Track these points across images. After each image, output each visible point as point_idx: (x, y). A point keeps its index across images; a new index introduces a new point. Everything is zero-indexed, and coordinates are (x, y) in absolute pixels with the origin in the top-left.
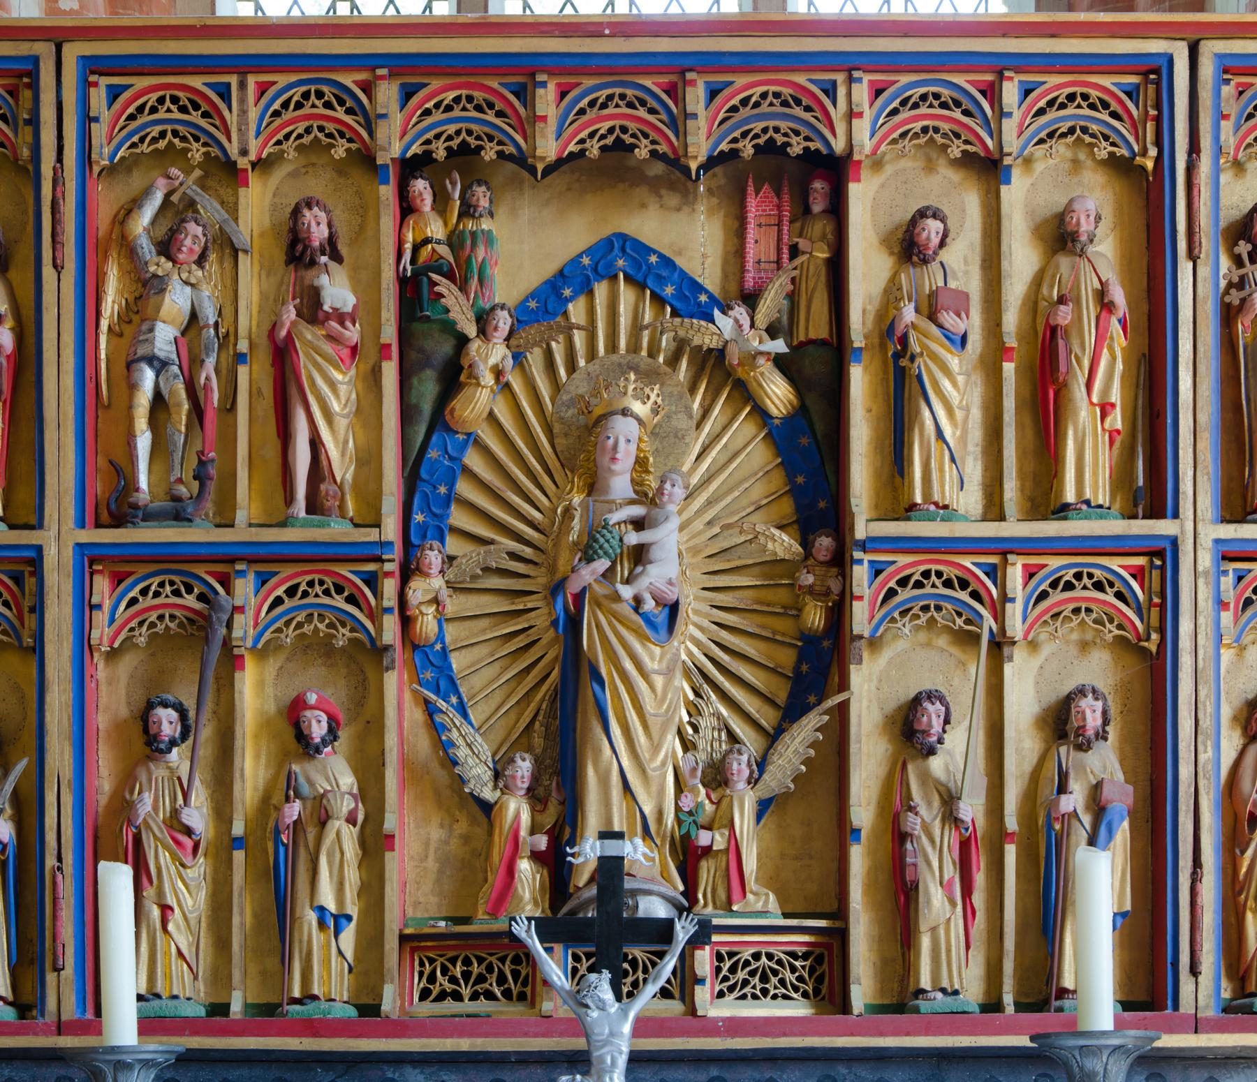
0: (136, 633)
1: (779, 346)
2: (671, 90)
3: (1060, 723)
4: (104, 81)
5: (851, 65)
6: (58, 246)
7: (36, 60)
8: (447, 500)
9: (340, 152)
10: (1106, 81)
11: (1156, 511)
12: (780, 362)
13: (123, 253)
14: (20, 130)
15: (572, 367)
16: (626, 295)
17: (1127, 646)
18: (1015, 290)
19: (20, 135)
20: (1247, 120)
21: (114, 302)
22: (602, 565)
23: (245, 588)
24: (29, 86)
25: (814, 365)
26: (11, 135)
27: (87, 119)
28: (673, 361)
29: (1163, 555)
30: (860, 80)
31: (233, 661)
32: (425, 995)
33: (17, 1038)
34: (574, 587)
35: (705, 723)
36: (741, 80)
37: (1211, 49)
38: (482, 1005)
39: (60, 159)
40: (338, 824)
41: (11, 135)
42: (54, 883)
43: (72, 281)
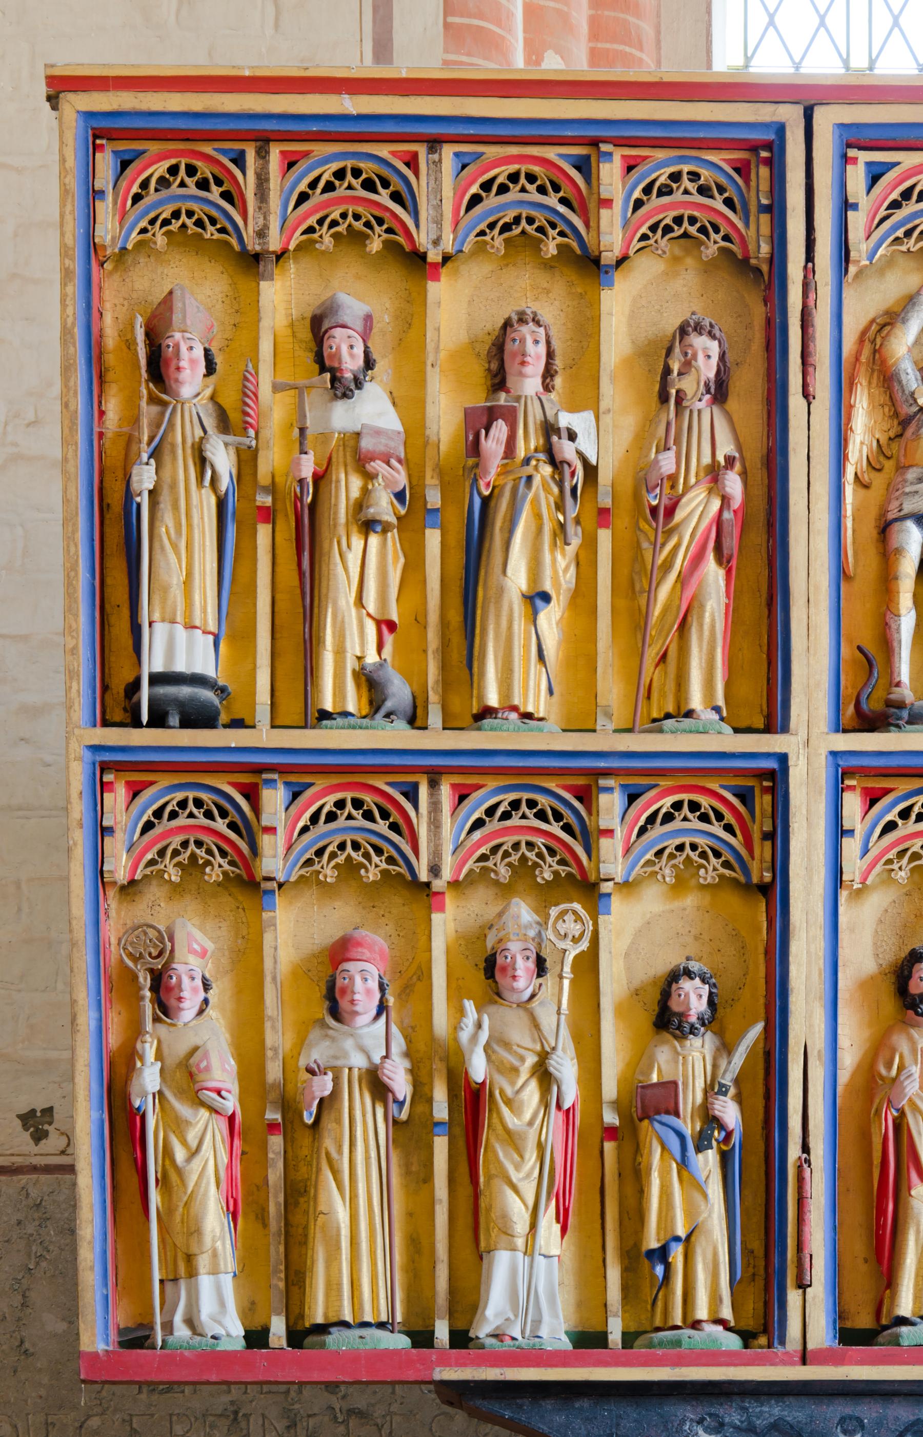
0: (895, 866)
2: (583, 166)
4: (864, 157)
6: (811, 369)
7: (781, 129)
9: (551, 248)
13: (875, 381)
14: (752, 219)
19: (753, 226)
20: (469, 208)
21: (862, 443)
24: (768, 162)
26: (740, 225)
27: (846, 206)
30: (855, 160)
33: (881, 1368)
39: (810, 256)
41: (740, 225)
42: (800, 1180)
43: (827, 414)
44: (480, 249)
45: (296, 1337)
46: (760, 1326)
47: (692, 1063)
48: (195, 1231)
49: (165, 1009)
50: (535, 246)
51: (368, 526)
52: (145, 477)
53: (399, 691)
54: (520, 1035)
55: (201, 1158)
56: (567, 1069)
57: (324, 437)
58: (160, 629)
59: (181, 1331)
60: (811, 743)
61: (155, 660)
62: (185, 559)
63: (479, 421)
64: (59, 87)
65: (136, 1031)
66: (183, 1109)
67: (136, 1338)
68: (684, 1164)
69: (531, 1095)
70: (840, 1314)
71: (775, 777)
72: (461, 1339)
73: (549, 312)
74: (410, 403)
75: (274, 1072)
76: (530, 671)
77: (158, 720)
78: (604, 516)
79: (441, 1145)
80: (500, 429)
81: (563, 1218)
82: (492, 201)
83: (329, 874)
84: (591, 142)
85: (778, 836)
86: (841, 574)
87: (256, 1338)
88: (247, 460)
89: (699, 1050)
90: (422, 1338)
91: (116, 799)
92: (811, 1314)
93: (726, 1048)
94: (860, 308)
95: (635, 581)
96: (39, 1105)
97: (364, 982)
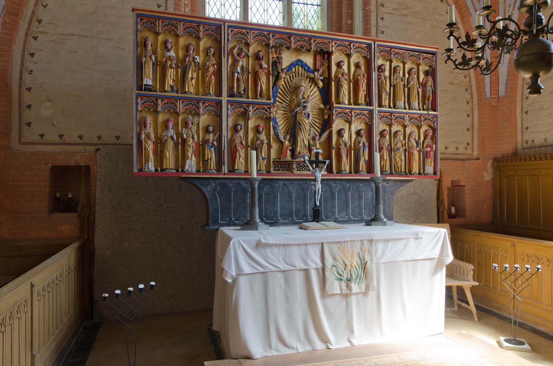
1: (322, 78)
2: (198, 26)
3: (358, 133)
5: (159, 18)
8: (276, 96)
10: (363, 45)
11: (370, 105)
12: (322, 80)
15: (293, 78)
16: (300, 68)
17: (366, 124)
18: (352, 73)
22: (300, 108)
23: (251, 108)
25: (326, 81)
27: (228, 35)
28: (307, 78)
29: (371, 112)
31: (249, 119)
32: (274, 170)
34: (296, 111)
35: (311, 131)
36: (318, 40)
37: (377, 43)
38: (283, 172)
40: (265, 144)
44: (185, 35)
45: (162, 170)
46: (219, 170)
47: (211, 137)
48: (149, 156)
49: (145, 127)
50: (192, 35)
51: (172, 68)
52: (144, 59)
53: (175, 88)
54: (190, 133)
55: (150, 147)
56: (196, 137)
57: (166, 56)
58: (145, 79)
59: (147, 169)
60: (225, 98)
61: (145, 83)
62: (149, 70)
63: (185, 56)
64: (133, 10)
65: (141, 130)
66: (148, 141)
67: (140, 170)
68: (210, 149)
69: (191, 140)
70: (228, 168)
71: (221, 102)
72: (182, 171)
73: (193, 43)
74: (177, 53)
75: (159, 136)
76: (191, 87)
77: (145, 90)
78: (200, 69)
79: (180, 146)
80: (188, 58)
81: (195, 156)
82: (187, 29)
83: (166, 111)
84: (199, 24)
85: (221, 109)
86: (228, 78)
87: (156, 170)
88: (156, 58)
89: (211, 135)
90: (178, 171)
91: (139, 100)
92: (225, 169)
93: (215, 135)
94: (230, 46)
95: (204, 77)
96: (62, 134)
97: (171, 125)
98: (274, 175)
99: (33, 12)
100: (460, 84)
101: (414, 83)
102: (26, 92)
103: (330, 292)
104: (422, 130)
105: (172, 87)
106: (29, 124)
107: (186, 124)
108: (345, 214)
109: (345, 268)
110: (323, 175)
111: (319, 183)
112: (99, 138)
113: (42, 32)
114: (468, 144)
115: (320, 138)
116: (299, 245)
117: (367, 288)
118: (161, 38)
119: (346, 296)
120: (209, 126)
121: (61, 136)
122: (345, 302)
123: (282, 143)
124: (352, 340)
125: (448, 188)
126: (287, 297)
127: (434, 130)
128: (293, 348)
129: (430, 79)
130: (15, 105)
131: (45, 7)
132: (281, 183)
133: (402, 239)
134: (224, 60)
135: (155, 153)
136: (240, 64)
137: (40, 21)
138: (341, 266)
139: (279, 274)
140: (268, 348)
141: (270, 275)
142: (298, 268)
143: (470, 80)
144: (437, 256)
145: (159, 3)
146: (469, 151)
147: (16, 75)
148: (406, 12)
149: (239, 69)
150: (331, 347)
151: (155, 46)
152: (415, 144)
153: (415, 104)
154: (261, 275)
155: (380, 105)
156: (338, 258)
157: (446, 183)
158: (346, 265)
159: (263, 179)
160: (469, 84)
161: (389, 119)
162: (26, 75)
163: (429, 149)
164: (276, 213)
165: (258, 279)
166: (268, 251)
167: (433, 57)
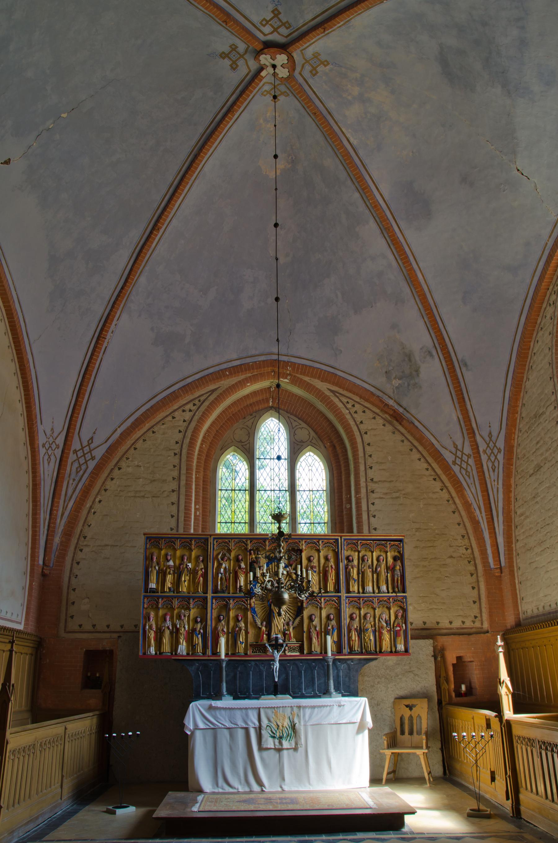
5: (162, 538)
17: (336, 608)
18: (322, 565)
23: (231, 601)
27: (214, 545)
29: (339, 597)
31: (229, 610)
37: (343, 538)
38: (260, 653)
40: (243, 631)
46: (204, 653)
52: (150, 569)
53: (172, 589)
54: (182, 623)
55: (152, 635)
62: (153, 577)
63: (180, 564)
64: (144, 534)
67: (144, 654)
69: (183, 629)
71: (206, 598)
72: (176, 654)
74: (174, 562)
75: (159, 626)
76: (184, 588)
77: (150, 592)
87: (156, 654)
88: (159, 568)
90: (172, 654)
91: (146, 600)
92: (209, 652)
93: (202, 624)
94: (215, 553)
95: (194, 578)
97: (168, 618)
98: (250, 656)
99: (81, 531)
100: (461, 557)
101: (382, 569)
102: (72, 592)
103: (265, 746)
104: (392, 612)
105: (169, 588)
106: (72, 617)
107: (179, 617)
108: (311, 690)
109: (278, 729)
110: (280, 656)
111: (277, 662)
112: (122, 626)
113: (86, 545)
114: (476, 617)
115: (293, 623)
116: (240, 709)
117: (296, 744)
118: (163, 552)
119: (279, 750)
120: (197, 617)
121: (94, 626)
122: (278, 755)
123: (260, 629)
124: (283, 786)
125: (453, 665)
126: (231, 749)
127: (405, 610)
128: (235, 788)
129: (399, 563)
130: (64, 602)
131: (89, 526)
132: (253, 663)
133: (327, 706)
134: (210, 565)
135: (155, 640)
136: (224, 566)
137: (85, 537)
138: (274, 726)
139: (225, 730)
140: (216, 786)
141: (219, 730)
142: (240, 726)
143: (473, 551)
144: (359, 721)
145: (172, 514)
146: (478, 624)
147: (66, 579)
148: (397, 494)
149: (222, 570)
150: (264, 789)
151: (158, 558)
152: (385, 625)
153: (384, 588)
154: (212, 731)
155: (348, 591)
156: (272, 720)
157: (451, 659)
158: (278, 726)
159: (230, 660)
160: (472, 556)
161: (356, 602)
162: (73, 578)
163: (398, 628)
164: (249, 689)
165: (210, 733)
166: (218, 713)
167: (400, 544)
